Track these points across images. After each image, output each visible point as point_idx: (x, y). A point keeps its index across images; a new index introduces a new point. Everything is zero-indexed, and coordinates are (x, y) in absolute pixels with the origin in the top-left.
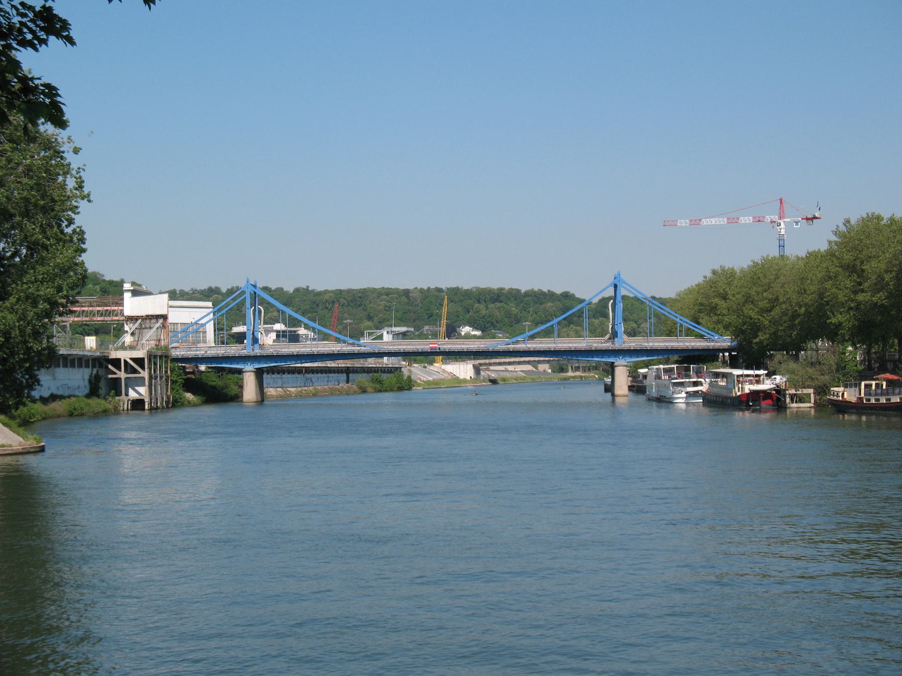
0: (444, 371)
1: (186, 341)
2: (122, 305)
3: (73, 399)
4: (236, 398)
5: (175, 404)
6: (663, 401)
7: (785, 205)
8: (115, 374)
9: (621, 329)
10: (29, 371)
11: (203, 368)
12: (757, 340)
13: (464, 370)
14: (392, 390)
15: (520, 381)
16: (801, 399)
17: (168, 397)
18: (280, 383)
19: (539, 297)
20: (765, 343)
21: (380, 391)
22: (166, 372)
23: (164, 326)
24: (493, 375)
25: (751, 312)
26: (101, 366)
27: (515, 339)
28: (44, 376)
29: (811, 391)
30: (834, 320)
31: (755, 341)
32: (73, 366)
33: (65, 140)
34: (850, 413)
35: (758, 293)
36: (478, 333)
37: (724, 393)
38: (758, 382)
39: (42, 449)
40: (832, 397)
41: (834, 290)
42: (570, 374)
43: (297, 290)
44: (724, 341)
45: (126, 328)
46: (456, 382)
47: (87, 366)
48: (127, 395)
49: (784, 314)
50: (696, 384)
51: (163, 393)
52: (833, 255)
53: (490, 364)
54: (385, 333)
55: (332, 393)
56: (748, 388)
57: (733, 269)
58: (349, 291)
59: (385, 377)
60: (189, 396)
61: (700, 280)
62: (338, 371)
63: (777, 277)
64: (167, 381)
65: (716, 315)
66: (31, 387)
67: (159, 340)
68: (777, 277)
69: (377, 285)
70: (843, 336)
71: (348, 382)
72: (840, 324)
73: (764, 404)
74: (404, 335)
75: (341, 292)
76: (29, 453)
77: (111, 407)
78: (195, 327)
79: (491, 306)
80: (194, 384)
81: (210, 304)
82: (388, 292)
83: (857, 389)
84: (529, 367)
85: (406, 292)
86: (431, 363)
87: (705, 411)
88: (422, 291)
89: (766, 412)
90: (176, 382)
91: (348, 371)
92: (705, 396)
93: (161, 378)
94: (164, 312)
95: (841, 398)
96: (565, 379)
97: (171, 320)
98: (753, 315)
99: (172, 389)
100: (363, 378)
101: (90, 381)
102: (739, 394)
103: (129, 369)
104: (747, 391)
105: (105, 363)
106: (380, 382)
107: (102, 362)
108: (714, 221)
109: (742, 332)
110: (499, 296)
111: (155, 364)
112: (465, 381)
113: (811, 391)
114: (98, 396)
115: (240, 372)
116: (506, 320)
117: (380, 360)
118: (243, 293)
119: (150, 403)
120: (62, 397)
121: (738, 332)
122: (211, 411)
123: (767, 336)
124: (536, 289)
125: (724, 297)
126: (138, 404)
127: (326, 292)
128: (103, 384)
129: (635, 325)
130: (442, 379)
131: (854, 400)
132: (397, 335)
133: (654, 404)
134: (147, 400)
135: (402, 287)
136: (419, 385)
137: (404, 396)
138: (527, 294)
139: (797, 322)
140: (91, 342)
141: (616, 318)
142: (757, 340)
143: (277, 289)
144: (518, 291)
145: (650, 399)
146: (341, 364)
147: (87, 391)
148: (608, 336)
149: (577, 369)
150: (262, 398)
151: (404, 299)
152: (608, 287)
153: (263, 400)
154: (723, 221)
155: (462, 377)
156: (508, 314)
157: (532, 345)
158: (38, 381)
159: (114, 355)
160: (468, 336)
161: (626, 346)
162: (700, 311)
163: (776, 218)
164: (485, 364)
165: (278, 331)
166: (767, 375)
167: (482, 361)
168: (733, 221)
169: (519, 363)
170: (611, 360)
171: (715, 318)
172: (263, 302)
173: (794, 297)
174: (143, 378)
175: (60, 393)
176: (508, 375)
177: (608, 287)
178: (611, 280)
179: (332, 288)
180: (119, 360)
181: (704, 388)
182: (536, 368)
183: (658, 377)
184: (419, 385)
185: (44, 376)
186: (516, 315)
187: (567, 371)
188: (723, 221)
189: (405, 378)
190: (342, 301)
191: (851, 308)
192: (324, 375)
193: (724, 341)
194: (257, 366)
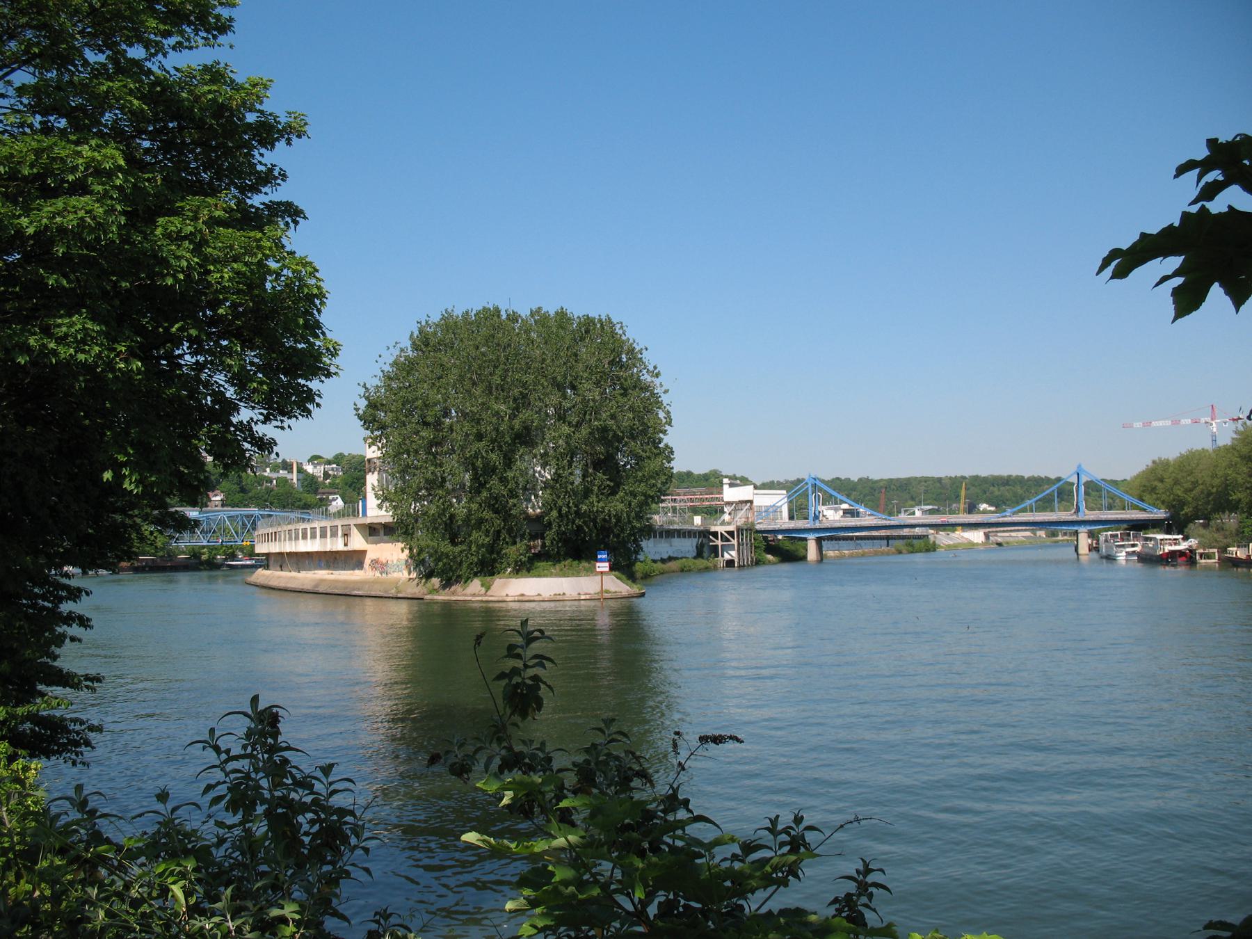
0: (962, 537)
1: (768, 518)
2: (722, 493)
3: (684, 559)
4: (804, 558)
5: (758, 563)
6: (1110, 558)
7: (1216, 410)
8: (714, 542)
9: (1083, 505)
10: (635, 541)
11: (780, 537)
12: (1183, 512)
13: (977, 536)
14: (921, 552)
15: (1021, 546)
16: (1208, 556)
17: (752, 558)
18: (837, 547)
19: (1039, 482)
20: (1189, 515)
21: (912, 552)
22: (750, 540)
23: (751, 508)
24: (1000, 540)
25: (1179, 491)
26: (705, 536)
27: (1004, 514)
28: (646, 544)
29: (1216, 550)
30: (1234, 497)
31: (1182, 513)
32: (684, 537)
33: (658, 385)
34: (1243, 567)
35: (1183, 477)
36: (993, 509)
37: (1151, 552)
38: (1175, 544)
39: (643, 595)
40: (1228, 555)
41: (1234, 475)
42: (1060, 538)
43: (860, 480)
44: (1161, 513)
45: (726, 510)
46: (971, 545)
47: (695, 537)
48: (723, 556)
49: (1202, 492)
50: (1133, 546)
51: (748, 555)
52: (1234, 449)
53: (997, 532)
54: (916, 511)
55: (876, 554)
56: (1168, 548)
57: (1168, 460)
58: (898, 480)
59: (915, 542)
60: (770, 557)
61: (1144, 468)
62: (881, 538)
63: (1198, 465)
64: (751, 546)
65: (1156, 494)
66: (637, 553)
67: (748, 518)
68: (1198, 465)
69: (918, 475)
70: (1242, 508)
71: (888, 546)
72: (1240, 500)
73: (1180, 560)
74: (931, 512)
75: (891, 480)
76: (633, 597)
77: (711, 565)
78: (774, 508)
79: (1002, 488)
80: (772, 549)
81: (784, 492)
82: (926, 480)
83: (1247, 549)
84: (1028, 534)
85: (940, 480)
86: (954, 531)
87: (1139, 565)
88: (951, 478)
89: (1180, 565)
90: (759, 547)
91: (888, 538)
92: (1139, 555)
93: (747, 545)
94: (750, 499)
95: (1234, 556)
96: (1057, 542)
97: (755, 504)
98: (1179, 493)
99: (755, 552)
100: (899, 543)
101: (697, 547)
102: (1161, 553)
103: (724, 538)
104: (1166, 551)
105: (707, 535)
106: (912, 546)
107: (705, 534)
108: (1161, 423)
109: (1174, 506)
110: (1008, 481)
111: (742, 534)
112: (977, 544)
113: (1216, 550)
114: (703, 558)
115: (805, 539)
116: (1013, 499)
117: (912, 530)
118: (807, 484)
119: (739, 563)
120: (676, 559)
121: (1170, 506)
122: (786, 567)
123: (1191, 509)
124: (1036, 475)
125: (1161, 480)
126: (730, 563)
127: (882, 480)
128: (706, 549)
129: (1111, 501)
130: (959, 544)
131: (1244, 557)
132: (924, 512)
133: (1104, 561)
134: (736, 560)
135: (937, 475)
136: (942, 547)
137: (932, 554)
138: (1030, 479)
139: (1210, 499)
140: (698, 520)
141: (1080, 496)
142: (1183, 512)
143: (846, 479)
144: (1023, 477)
145: (1102, 557)
146: (883, 533)
147: (695, 554)
148: (1073, 511)
149: (1065, 534)
150: (821, 558)
151: (938, 485)
152: (1072, 475)
153: (822, 560)
154: (1168, 423)
155: (975, 542)
156: (1015, 495)
157: (1016, 519)
158: (642, 549)
159: (713, 529)
160: (985, 512)
161: (1086, 518)
162: (1144, 491)
163: (1209, 419)
164: (993, 532)
165: (844, 510)
166: (1183, 539)
167: (990, 530)
168: (1176, 422)
169: (1018, 531)
170: (1075, 528)
171: (1155, 496)
172: (821, 490)
173: (1208, 480)
174: (734, 545)
175: (675, 556)
176: (1011, 539)
177: (1072, 475)
178: (1074, 469)
179: (886, 477)
180: (717, 532)
181: (1137, 549)
182: (1035, 534)
183: (1106, 541)
184: (942, 547)
185: (646, 544)
186: (1021, 495)
187: (1057, 536)
188: (1168, 423)
189: (931, 542)
190: (892, 487)
191: (1247, 488)
192: (870, 541)
193: (1160, 514)
194: (817, 536)
